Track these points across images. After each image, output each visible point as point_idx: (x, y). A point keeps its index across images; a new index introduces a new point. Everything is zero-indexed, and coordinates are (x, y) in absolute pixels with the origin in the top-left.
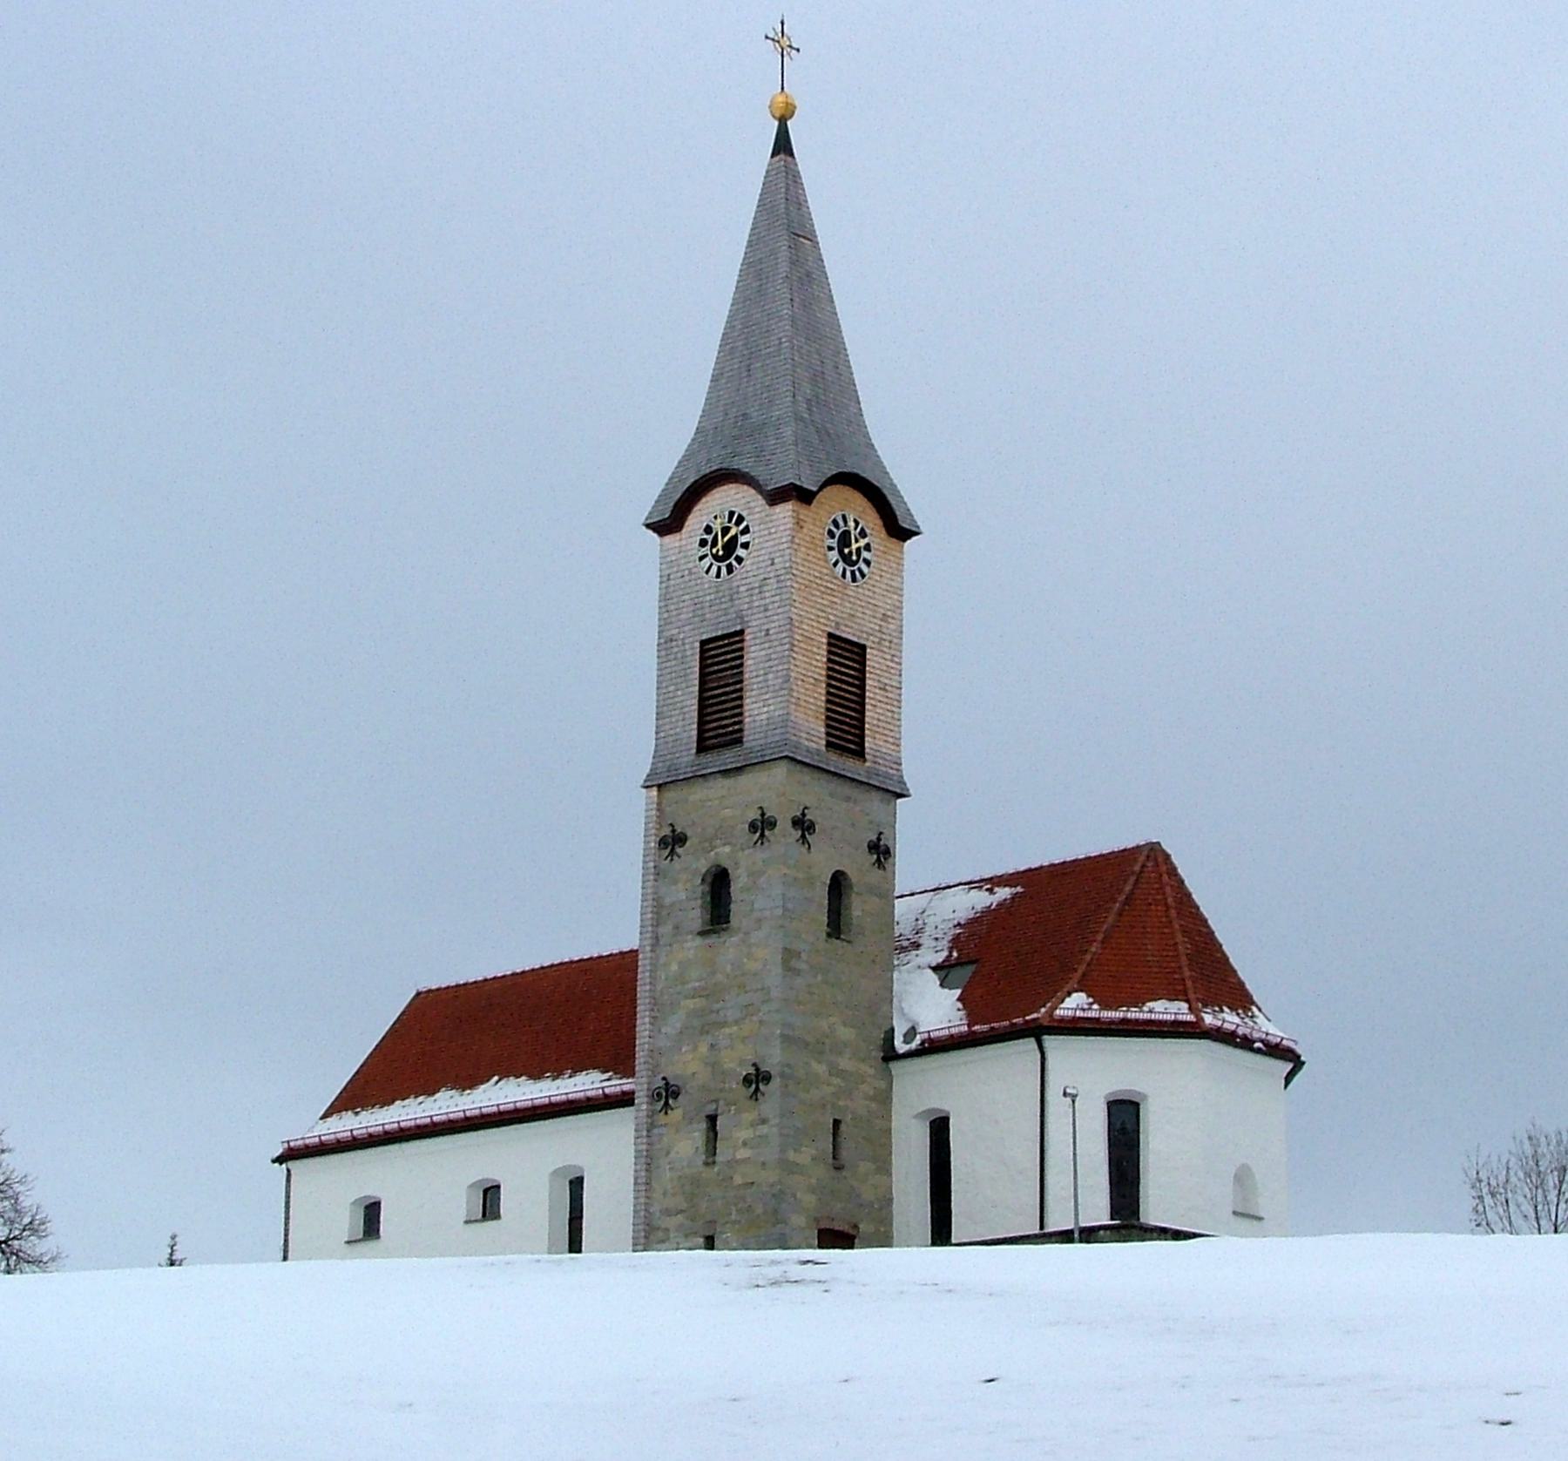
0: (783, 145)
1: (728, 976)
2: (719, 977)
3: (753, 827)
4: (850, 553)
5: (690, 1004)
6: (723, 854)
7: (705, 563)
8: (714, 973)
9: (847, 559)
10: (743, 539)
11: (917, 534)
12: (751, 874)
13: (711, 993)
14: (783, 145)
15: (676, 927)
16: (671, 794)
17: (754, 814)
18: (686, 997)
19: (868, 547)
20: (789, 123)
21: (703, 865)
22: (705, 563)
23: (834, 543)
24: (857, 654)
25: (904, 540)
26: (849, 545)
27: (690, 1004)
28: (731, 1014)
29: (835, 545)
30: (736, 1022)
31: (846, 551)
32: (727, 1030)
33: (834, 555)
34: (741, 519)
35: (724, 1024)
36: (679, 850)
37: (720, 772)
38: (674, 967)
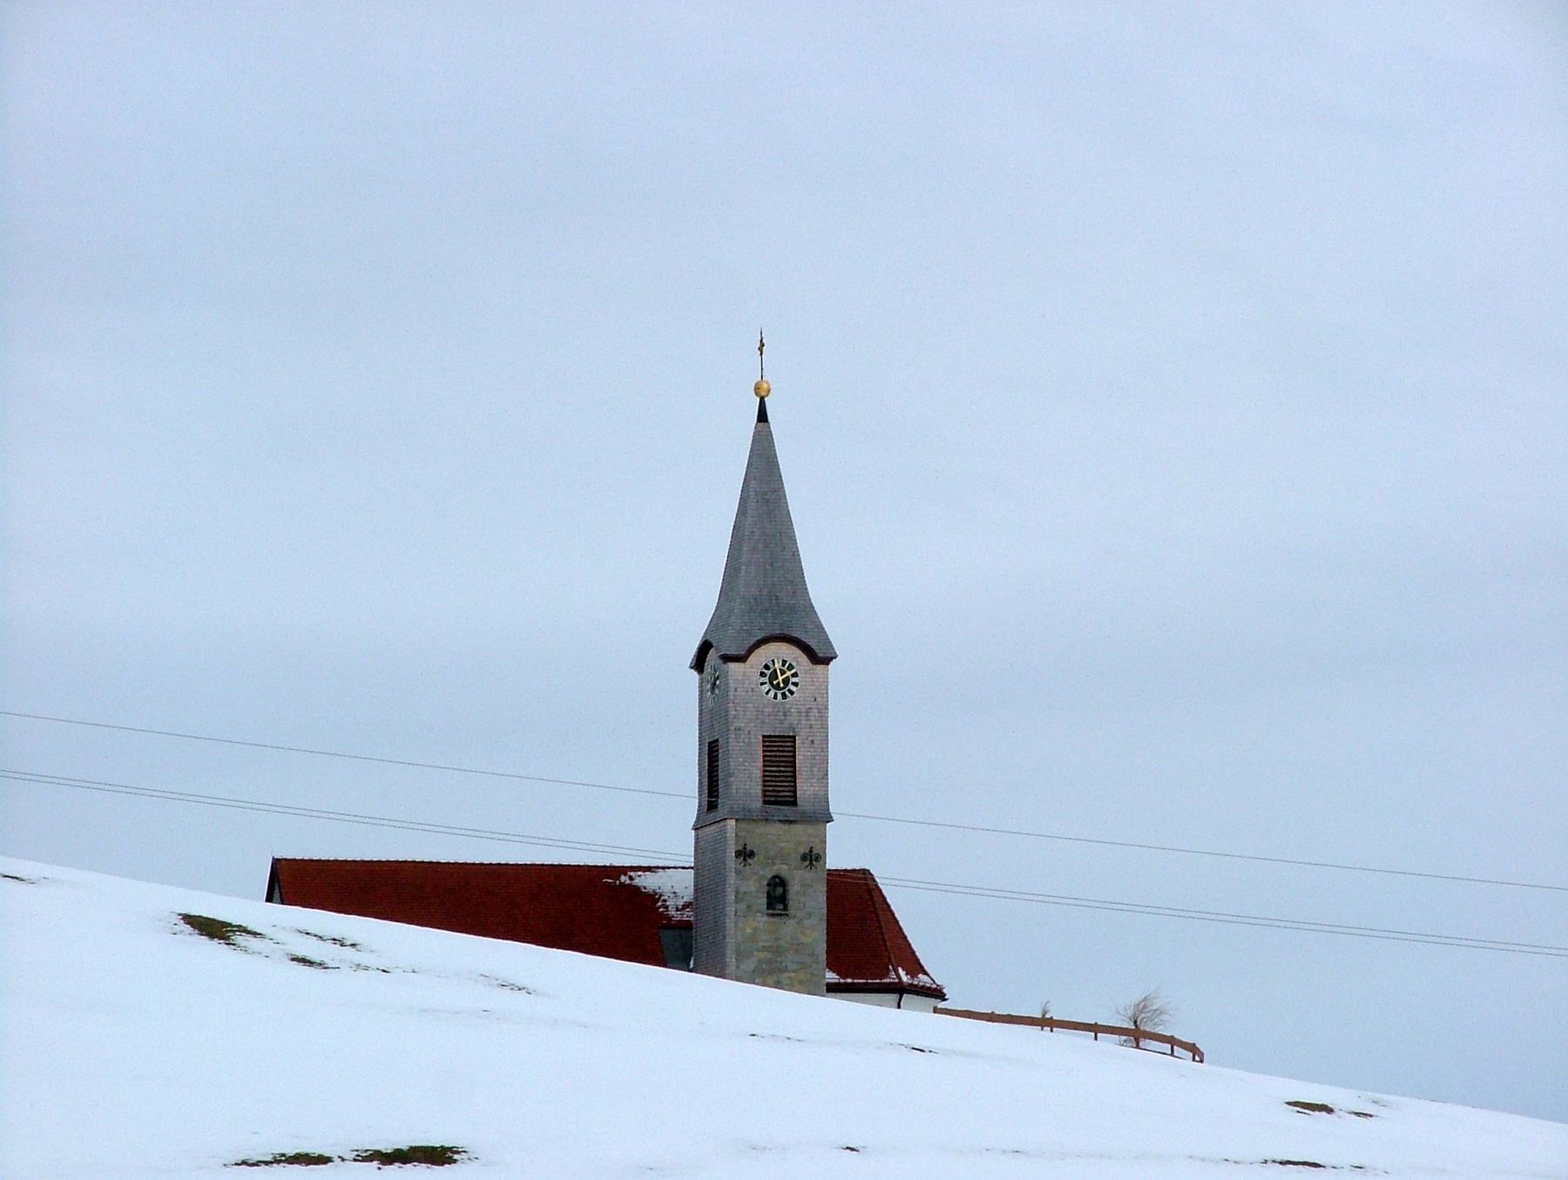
0: (762, 416)
1: (787, 943)
2: (781, 942)
3: (804, 858)
4: (778, 683)
5: (762, 955)
6: (783, 869)
7: (765, 688)
8: (777, 939)
9: (777, 687)
10: (794, 680)
11: (835, 658)
12: (803, 885)
13: (777, 951)
14: (762, 416)
15: (748, 907)
16: (700, 832)
17: (803, 850)
18: (758, 950)
19: (795, 675)
20: (766, 399)
21: (769, 873)
22: (765, 688)
23: (766, 679)
24: (791, 742)
25: (828, 664)
26: (777, 678)
27: (762, 955)
28: (791, 966)
29: (767, 681)
30: (794, 971)
31: (775, 682)
32: (786, 975)
33: (767, 687)
34: (791, 667)
35: (786, 970)
36: (750, 861)
37: (779, 821)
38: (749, 931)
